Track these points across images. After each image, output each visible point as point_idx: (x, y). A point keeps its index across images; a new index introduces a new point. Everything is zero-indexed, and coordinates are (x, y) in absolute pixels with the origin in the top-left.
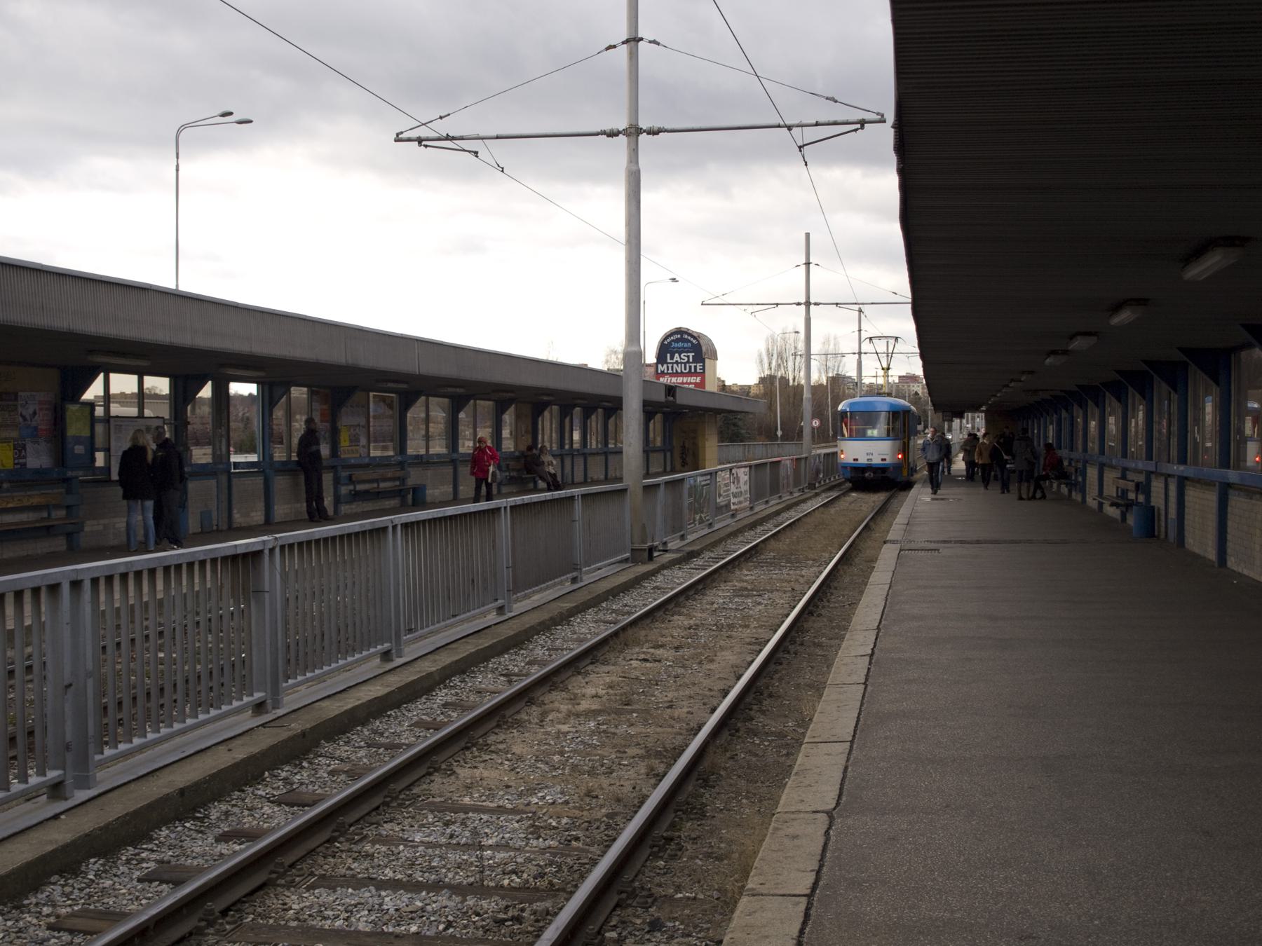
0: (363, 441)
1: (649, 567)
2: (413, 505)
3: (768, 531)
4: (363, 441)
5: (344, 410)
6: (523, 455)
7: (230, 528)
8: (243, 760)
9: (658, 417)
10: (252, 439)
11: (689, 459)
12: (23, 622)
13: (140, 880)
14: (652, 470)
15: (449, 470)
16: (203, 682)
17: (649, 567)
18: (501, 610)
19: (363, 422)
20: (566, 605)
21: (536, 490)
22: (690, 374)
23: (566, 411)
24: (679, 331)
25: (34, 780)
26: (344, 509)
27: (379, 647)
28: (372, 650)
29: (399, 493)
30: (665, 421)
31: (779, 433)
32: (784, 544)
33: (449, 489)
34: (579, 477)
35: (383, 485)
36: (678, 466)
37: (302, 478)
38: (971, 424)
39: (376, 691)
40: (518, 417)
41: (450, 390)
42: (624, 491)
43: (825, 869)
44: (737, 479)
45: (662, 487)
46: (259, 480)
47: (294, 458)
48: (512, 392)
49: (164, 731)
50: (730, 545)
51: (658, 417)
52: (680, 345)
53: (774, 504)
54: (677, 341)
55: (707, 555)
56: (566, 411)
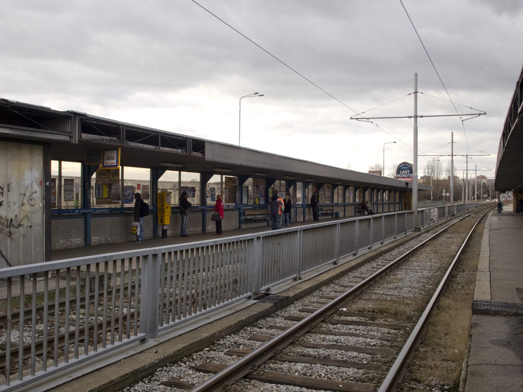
0: (324, 199)
1: (419, 233)
2: (314, 220)
3: (445, 227)
4: (324, 199)
5: (321, 189)
6: (361, 204)
7: (304, 220)
8: (207, 337)
9: (398, 192)
10: (119, 197)
11: (407, 207)
12: (124, 269)
13: (299, 311)
14: (396, 210)
15: (80, 222)
16: (222, 289)
17: (419, 233)
18: (382, 243)
19: (323, 193)
20: (404, 240)
21: (364, 215)
22: (408, 177)
23: (372, 190)
24: (404, 163)
25: (132, 338)
26: (243, 226)
27: (293, 276)
28: (290, 277)
29: (332, 214)
30: (400, 193)
31: (432, 198)
32: (452, 229)
33: (200, 229)
34: (375, 211)
35: (258, 217)
36: (403, 208)
37: (311, 209)
38: (509, 196)
39: (353, 264)
40: (360, 192)
41: (287, 177)
42: (413, 212)
43: (471, 350)
44: (435, 211)
45: (383, 218)
46: (302, 209)
47: (310, 203)
48: (293, 176)
49: (221, 304)
50: (437, 229)
51: (398, 192)
52: (405, 168)
53: (443, 220)
54: (404, 166)
55: (432, 231)
56: (372, 190)
